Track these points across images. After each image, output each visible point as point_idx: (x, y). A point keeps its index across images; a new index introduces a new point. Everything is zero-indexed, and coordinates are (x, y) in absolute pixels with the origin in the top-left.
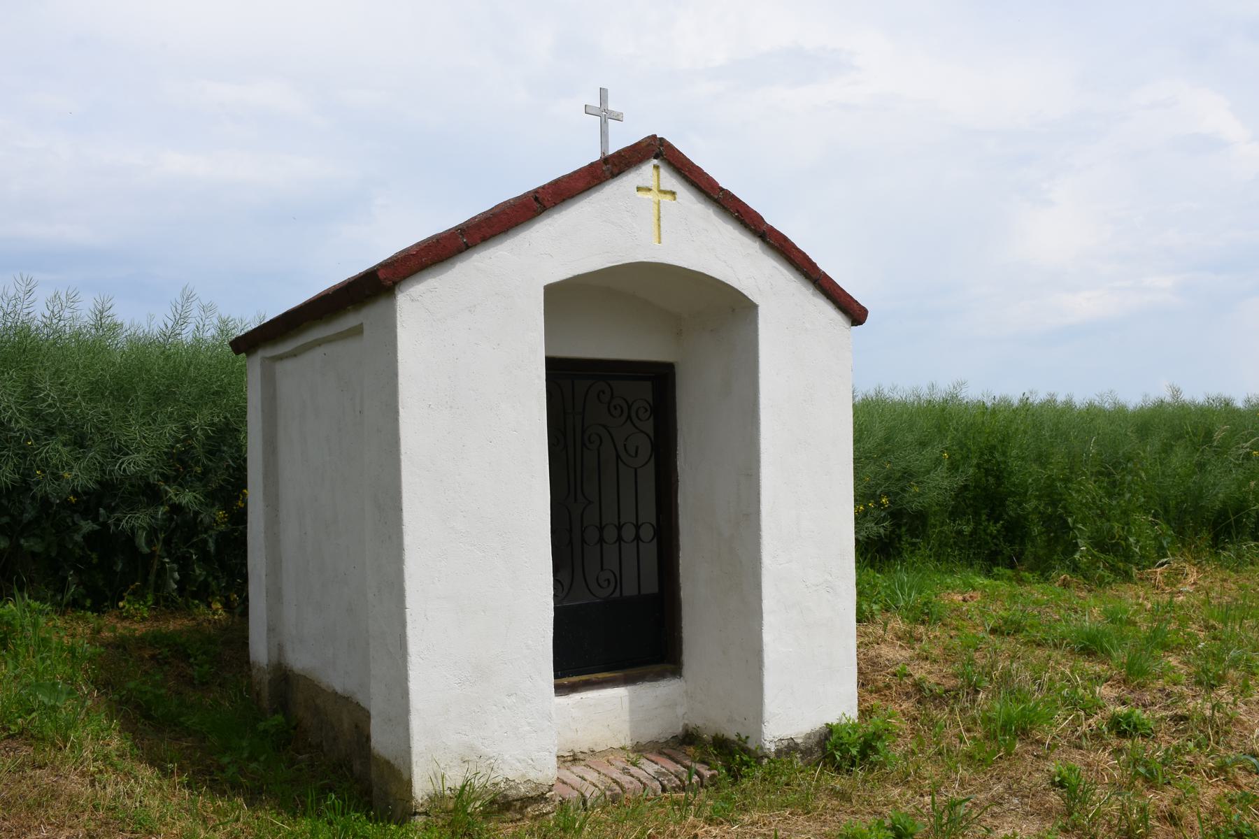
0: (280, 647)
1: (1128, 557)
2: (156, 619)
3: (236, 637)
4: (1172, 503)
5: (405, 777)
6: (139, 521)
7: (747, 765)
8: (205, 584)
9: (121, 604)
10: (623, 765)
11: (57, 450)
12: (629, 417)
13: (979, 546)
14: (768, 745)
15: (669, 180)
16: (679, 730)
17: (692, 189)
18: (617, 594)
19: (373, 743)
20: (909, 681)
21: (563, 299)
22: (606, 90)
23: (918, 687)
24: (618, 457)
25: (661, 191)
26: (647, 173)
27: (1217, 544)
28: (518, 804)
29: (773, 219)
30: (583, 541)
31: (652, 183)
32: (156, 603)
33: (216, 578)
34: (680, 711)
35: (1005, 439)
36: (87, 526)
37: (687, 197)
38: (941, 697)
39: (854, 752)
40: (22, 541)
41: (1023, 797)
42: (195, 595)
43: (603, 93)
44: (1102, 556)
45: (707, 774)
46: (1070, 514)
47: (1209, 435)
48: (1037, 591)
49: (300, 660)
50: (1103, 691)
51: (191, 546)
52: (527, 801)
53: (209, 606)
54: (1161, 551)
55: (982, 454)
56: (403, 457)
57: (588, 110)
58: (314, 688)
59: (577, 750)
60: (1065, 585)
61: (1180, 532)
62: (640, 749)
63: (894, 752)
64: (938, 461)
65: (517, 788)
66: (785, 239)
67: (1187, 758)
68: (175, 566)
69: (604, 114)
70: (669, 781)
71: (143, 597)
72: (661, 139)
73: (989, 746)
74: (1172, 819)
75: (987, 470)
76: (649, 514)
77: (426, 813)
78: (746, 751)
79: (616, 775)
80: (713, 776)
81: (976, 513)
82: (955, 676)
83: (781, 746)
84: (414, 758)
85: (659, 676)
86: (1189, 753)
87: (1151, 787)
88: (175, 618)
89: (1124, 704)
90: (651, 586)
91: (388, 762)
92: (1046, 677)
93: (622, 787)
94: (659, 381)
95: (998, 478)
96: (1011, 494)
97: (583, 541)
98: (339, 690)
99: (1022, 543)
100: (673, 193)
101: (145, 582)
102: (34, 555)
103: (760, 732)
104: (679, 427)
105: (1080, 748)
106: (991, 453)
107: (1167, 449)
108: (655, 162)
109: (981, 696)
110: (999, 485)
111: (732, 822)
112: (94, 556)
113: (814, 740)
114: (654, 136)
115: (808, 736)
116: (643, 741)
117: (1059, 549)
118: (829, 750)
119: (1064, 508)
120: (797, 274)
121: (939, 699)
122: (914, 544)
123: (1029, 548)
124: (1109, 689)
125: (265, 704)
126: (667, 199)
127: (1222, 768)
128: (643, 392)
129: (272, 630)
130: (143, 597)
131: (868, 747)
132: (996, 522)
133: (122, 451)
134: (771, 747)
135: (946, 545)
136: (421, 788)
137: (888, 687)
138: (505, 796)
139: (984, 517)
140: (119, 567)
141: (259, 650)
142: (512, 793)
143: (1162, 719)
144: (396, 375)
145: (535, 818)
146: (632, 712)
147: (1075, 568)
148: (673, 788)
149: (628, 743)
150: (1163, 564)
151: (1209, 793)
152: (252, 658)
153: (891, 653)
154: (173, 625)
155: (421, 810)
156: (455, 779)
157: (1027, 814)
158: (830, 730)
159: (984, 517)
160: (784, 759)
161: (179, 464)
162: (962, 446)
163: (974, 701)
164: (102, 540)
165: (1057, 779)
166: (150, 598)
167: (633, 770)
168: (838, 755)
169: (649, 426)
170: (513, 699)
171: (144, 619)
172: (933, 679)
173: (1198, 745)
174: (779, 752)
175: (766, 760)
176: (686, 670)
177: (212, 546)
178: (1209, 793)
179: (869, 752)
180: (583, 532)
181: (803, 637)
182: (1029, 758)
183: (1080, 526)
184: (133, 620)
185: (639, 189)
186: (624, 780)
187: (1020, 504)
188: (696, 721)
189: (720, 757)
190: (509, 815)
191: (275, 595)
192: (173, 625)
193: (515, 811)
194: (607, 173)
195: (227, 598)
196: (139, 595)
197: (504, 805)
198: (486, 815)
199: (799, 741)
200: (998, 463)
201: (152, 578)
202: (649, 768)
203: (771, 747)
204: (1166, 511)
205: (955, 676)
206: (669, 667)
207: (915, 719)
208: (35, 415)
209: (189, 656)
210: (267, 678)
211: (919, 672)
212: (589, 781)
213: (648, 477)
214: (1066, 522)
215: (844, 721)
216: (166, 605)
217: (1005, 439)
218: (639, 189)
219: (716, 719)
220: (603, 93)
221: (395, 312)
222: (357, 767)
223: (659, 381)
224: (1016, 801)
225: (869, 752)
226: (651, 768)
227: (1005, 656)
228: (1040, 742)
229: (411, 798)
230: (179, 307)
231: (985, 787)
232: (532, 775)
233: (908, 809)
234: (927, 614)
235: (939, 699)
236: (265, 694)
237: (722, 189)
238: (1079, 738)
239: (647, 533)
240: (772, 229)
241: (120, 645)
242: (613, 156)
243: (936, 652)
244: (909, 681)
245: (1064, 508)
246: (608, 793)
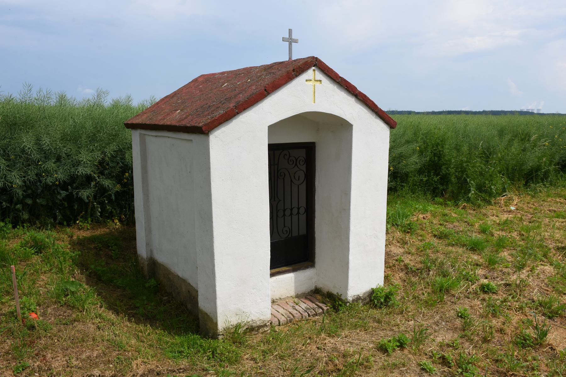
0: (151, 251)
1: (490, 194)
2: (93, 228)
3: (128, 236)
4: (510, 167)
5: (215, 321)
6: (85, 194)
7: (341, 306)
8: (111, 212)
9: (78, 222)
10: (292, 305)
11: (51, 165)
12: (296, 164)
13: (429, 186)
14: (349, 298)
15: (319, 75)
16: (313, 288)
17: (328, 78)
18: (290, 236)
19: (199, 305)
20: (402, 264)
22: (291, 30)
23: (406, 266)
24: (291, 181)
25: (315, 81)
26: (311, 73)
27: (526, 185)
28: (257, 328)
30: (277, 216)
31: (312, 77)
32: (92, 221)
33: (115, 209)
34: (314, 281)
35: (443, 141)
36: (64, 193)
37: (326, 82)
39: (382, 300)
40: (37, 200)
41: (447, 321)
42: (108, 218)
43: (290, 31)
44: (480, 194)
45: (325, 308)
46: (468, 177)
47: (528, 135)
48: (453, 213)
49: (161, 258)
50: (480, 272)
51: (105, 197)
52: (259, 327)
53: (113, 221)
54: (504, 190)
55: (433, 147)
56: (213, 202)
57: (284, 39)
58: (167, 272)
59: (274, 298)
60: (464, 208)
61: (512, 179)
62: (298, 296)
63: (396, 299)
64: (414, 151)
65: (256, 323)
66: (365, 96)
67: (509, 304)
68: (99, 206)
69: (290, 40)
70: (311, 312)
71: (86, 219)
72: (316, 58)
73: (435, 297)
74: (501, 331)
75: (434, 154)
76: (303, 203)
77: (223, 335)
78: (340, 300)
79: (291, 310)
80: (327, 309)
81: (429, 172)
82: (421, 262)
83: (354, 298)
84: (218, 315)
85: (306, 267)
86: (509, 301)
87: (494, 317)
88: (100, 228)
89: (486, 278)
90: (303, 231)
91: (207, 314)
92: (457, 265)
93: (294, 316)
94: (309, 149)
95: (439, 157)
96: (444, 164)
97: (277, 216)
98: (180, 275)
99: (447, 185)
100: (320, 81)
101: (86, 212)
102: (42, 206)
103: (347, 293)
104: (316, 168)
105: (469, 298)
106: (437, 146)
107: (511, 141)
108: (313, 68)
109: (431, 273)
110: (439, 160)
111: (338, 336)
112: (66, 204)
113: (367, 295)
114: (314, 57)
115: (365, 294)
116: (300, 293)
117: (463, 191)
118: (373, 299)
119: (467, 174)
120: (369, 110)
121: (414, 273)
122: (402, 186)
123: (450, 188)
124: (481, 270)
125: (146, 273)
126: (318, 84)
127: (521, 308)
128: (302, 153)
129: (148, 244)
130: (86, 219)
131: (387, 297)
132: (437, 176)
133: (79, 163)
134: (350, 299)
135: (415, 185)
136: (221, 325)
137: (394, 266)
138: (252, 326)
139: (432, 174)
140: (76, 207)
141: (142, 250)
142: (254, 325)
143: (500, 285)
144: (210, 168)
145: (262, 333)
146: (295, 282)
147: (468, 200)
148: (313, 315)
149: (293, 293)
150: (504, 196)
151: (515, 318)
152: (139, 252)
153: (397, 250)
154: (100, 231)
155: (221, 333)
156: (234, 321)
157: (448, 329)
158: (373, 291)
159: (432, 174)
160: (356, 303)
161: (102, 167)
162: (425, 142)
163: (428, 274)
164: (69, 198)
165: (460, 314)
166: (89, 219)
167: (297, 307)
168: (376, 301)
169: (304, 168)
170: (255, 290)
171: (88, 229)
172: (412, 264)
173: (513, 298)
174: (353, 301)
175: (348, 304)
176: (316, 265)
177: (113, 197)
178: (515, 318)
179: (388, 300)
180: (277, 213)
181: (364, 256)
182: (449, 303)
183: (472, 182)
184: (83, 231)
185: (306, 81)
186: (294, 312)
187: (447, 169)
188: (320, 285)
189: (329, 300)
190: (253, 333)
191: (149, 231)
192: (100, 231)
195: (120, 217)
196: (85, 219)
197: (252, 329)
198: (245, 333)
199: (361, 296)
200: (440, 151)
201: (89, 211)
202: (304, 305)
203: (350, 299)
204: (508, 170)
205: (421, 262)
207: (405, 281)
208: (41, 150)
209: (109, 246)
210: (146, 263)
211: (407, 260)
212: (282, 314)
213: (303, 188)
214: (466, 180)
215: (378, 287)
216: (97, 223)
217: (443, 141)
218: (306, 81)
219: (329, 285)
220: (290, 31)
221: (209, 143)
222: (189, 306)
223: (309, 149)
224: (444, 323)
225: (388, 300)
226: (304, 306)
227: (441, 251)
228: (453, 296)
229: (217, 329)
230: (96, 97)
231: (432, 317)
232: (262, 318)
233: (402, 328)
234: (409, 229)
235: (414, 273)
236: (146, 268)
237: (340, 77)
238: (468, 293)
239: (302, 210)
240: (360, 93)
241: (80, 244)
242: (295, 61)
243: (413, 251)
244: (402, 264)
245: (467, 174)
246: (288, 319)
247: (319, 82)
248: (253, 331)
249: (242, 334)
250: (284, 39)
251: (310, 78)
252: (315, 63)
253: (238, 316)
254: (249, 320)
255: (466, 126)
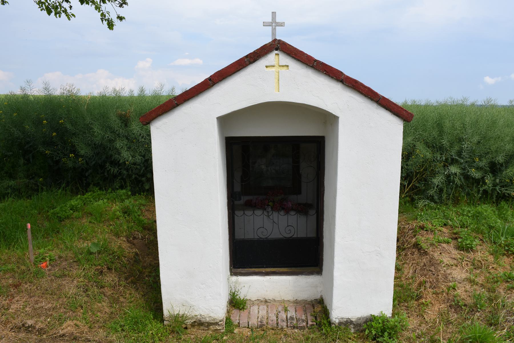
15: (284, 59)
16: (318, 297)
21: (224, 121)
25: (280, 66)
26: (272, 58)
28: (206, 324)
29: (348, 72)
31: (274, 63)
34: (319, 289)
38: (461, 307)
43: (274, 14)
52: (209, 324)
59: (267, 298)
72: (279, 40)
83: (342, 321)
108: (276, 52)
115: (359, 319)
116: (299, 299)
138: (200, 321)
142: (203, 320)
174: (340, 323)
181: (361, 275)
185: (267, 67)
190: (202, 328)
193: (205, 326)
194: (247, 62)
199: (353, 320)
206: (317, 269)
218: (267, 67)
220: (274, 14)
232: (212, 315)
247: (285, 68)
248: (202, 325)
249: (180, 325)
250: (265, 24)
251: (272, 64)
252: (278, 46)
253: (185, 307)
254: (197, 313)
255: (142, 90)
